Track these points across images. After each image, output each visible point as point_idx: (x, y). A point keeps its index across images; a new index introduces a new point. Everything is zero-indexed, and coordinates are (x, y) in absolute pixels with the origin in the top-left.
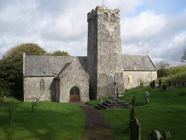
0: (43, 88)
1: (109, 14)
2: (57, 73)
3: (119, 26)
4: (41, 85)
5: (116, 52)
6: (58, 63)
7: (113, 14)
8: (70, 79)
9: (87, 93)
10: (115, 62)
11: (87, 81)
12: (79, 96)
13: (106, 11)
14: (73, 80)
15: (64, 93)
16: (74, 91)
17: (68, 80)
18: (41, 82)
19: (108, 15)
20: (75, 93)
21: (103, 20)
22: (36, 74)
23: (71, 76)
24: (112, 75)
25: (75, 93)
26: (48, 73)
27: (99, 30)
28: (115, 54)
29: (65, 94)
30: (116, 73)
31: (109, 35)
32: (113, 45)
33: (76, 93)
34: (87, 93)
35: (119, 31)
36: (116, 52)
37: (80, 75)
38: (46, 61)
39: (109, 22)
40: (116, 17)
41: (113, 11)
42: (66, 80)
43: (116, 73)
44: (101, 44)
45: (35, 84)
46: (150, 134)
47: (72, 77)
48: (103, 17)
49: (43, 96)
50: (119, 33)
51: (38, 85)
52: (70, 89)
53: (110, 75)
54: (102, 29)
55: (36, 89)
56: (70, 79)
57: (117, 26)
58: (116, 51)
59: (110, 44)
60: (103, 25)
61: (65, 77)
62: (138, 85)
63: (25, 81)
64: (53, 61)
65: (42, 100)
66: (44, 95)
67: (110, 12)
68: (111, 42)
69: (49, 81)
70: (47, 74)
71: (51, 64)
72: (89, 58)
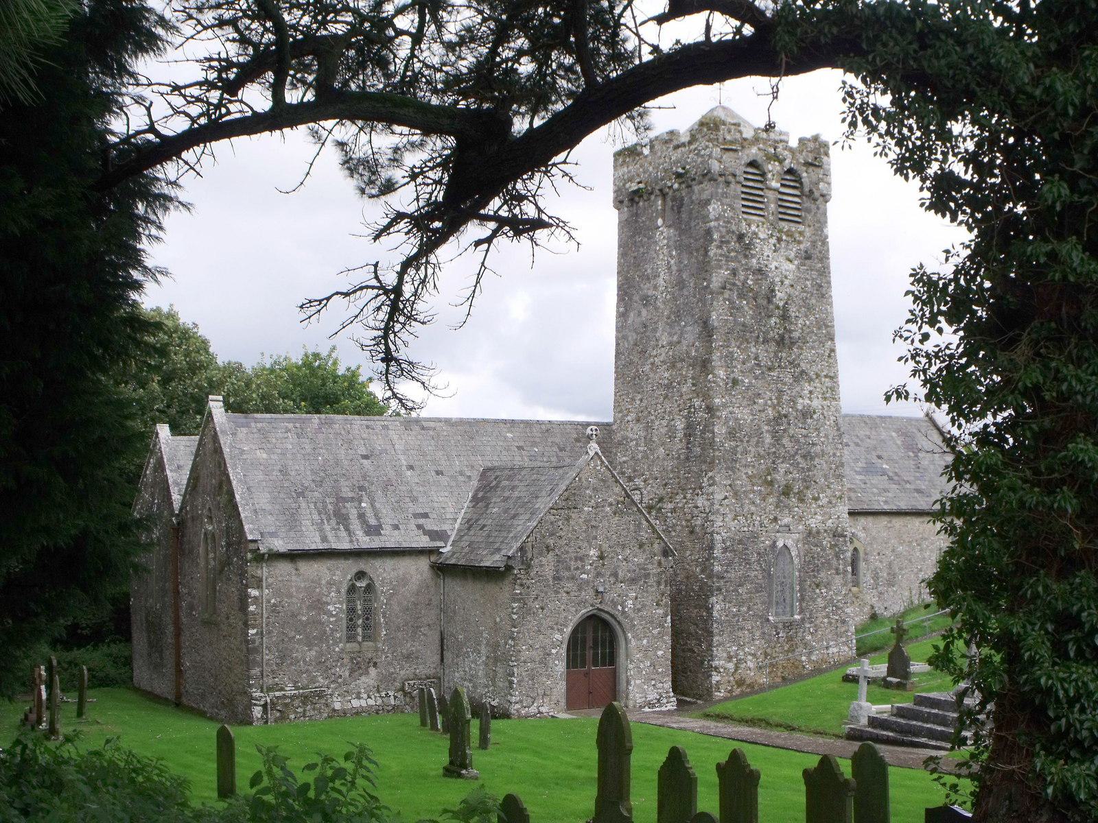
1: (773, 167)
2: (446, 527)
3: (824, 242)
4: (351, 610)
5: (807, 401)
7: (790, 171)
8: (568, 569)
9: (660, 653)
10: (803, 464)
11: (659, 583)
13: (754, 150)
14: (585, 576)
16: (590, 643)
17: (557, 578)
18: (352, 589)
19: (770, 176)
20: (589, 654)
22: (324, 539)
24: (790, 543)
25: (589, 654)
26: (396, 527)
27: (720, 267)
28: (807, 414)
29: (543, 662)
33: (595, 655)
34: (660, 653)
35: (824, 272)
36: (807, 401)
37: (624, 547)
39: (771, 218)
40: (806, 190)
41: (791, 150)
42: (549, 572)
44: (730, 356)
45: (319, 605)
47: (581, 559)
48: (740, 189)
49: (363, 678)
50: (821, 289)
51: (336, 606)
52: (568, 630)
53: (780, 544)
54: (735, 259)
55: (323, 637)
56: (568, 569)
57: (814, 243)
60: (741, 237)
65: (363, 703)
66: (373, 671)
69: (404, 581)
70: (390, 539)
71: (399, 474)
72: (635, 432)
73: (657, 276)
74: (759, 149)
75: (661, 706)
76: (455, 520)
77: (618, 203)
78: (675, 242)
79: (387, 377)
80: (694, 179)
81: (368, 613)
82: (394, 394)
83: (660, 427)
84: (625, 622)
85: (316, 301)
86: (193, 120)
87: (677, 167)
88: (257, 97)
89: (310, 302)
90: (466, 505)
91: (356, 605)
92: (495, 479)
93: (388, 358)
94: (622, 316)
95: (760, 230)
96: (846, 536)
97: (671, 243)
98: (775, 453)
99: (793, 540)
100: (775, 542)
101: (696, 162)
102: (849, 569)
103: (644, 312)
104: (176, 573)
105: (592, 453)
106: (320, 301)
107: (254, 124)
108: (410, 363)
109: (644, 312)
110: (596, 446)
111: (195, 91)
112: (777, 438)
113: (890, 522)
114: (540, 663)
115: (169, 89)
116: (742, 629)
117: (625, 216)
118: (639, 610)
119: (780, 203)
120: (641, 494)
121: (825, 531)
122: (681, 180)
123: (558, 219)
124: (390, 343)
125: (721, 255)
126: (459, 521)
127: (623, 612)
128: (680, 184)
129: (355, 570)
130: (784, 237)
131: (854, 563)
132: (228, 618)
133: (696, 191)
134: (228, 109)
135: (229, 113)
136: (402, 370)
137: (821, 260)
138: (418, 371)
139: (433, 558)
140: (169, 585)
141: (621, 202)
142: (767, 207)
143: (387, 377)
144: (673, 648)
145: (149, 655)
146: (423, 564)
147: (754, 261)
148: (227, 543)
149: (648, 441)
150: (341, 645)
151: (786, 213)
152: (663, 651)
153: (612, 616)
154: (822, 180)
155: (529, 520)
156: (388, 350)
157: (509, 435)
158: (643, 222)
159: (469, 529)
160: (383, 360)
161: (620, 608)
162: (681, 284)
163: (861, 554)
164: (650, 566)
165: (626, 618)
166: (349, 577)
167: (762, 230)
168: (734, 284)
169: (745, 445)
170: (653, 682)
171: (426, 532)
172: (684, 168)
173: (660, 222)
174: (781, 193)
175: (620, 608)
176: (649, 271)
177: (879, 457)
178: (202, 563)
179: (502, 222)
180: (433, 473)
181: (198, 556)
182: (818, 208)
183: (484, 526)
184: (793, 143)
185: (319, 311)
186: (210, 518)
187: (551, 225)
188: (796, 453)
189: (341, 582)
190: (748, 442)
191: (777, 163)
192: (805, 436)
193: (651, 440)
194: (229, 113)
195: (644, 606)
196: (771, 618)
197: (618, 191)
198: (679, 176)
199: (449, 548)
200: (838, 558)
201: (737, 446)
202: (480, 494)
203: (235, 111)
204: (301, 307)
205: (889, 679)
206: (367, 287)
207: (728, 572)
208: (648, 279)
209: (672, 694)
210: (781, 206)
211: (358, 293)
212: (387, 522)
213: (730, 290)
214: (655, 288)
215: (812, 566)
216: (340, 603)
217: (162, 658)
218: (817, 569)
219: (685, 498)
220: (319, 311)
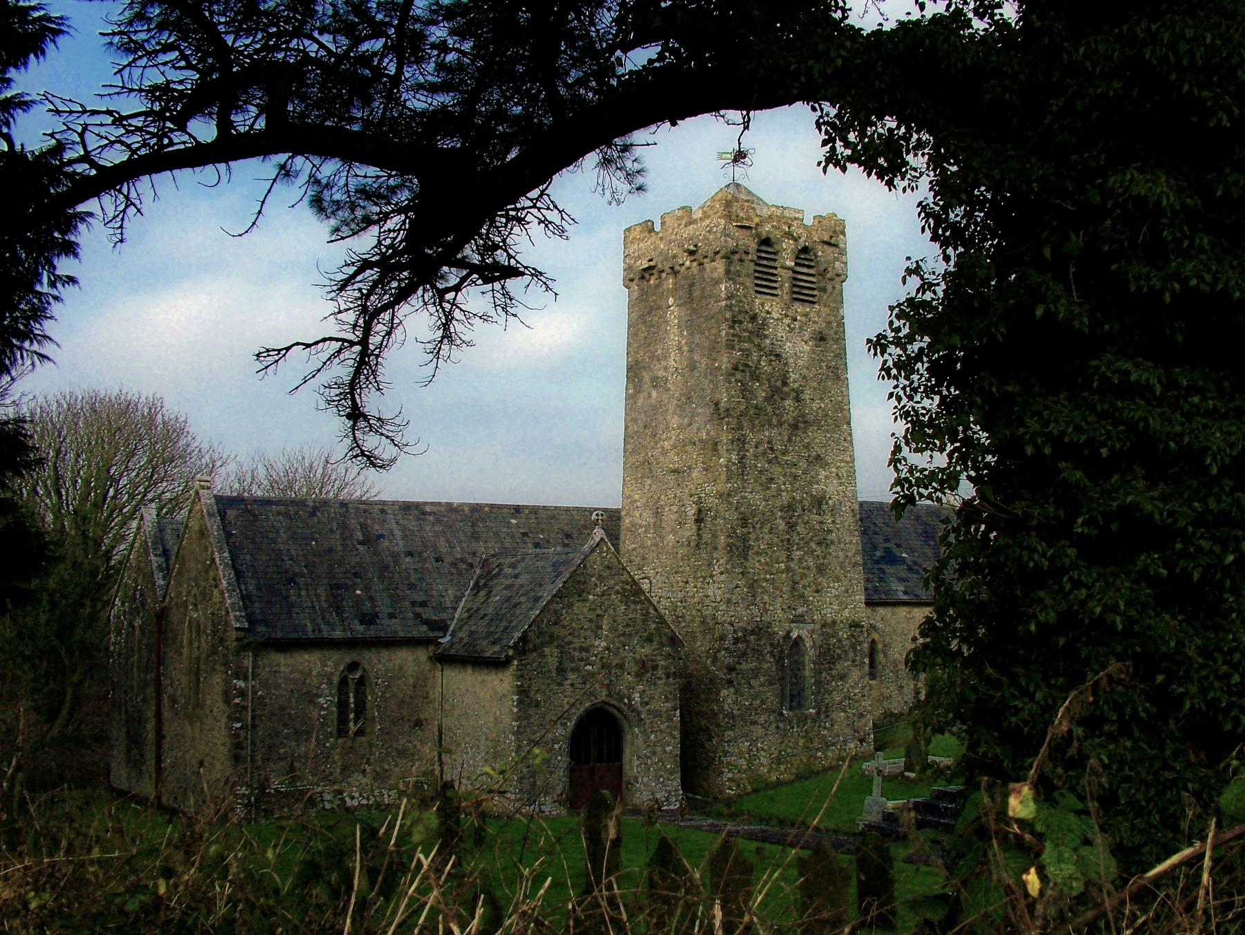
3: (841, 324)
4: (342, 706)
6: (435, 548)
9: (668, 749)
11: (668, 676)
14: (589, 668)
17: (561, 670)
18: (344, 682)
21: (749, 283)
23: (577, 643)
24: (804, 633)
31: (785, 384)
32: (807, 447)
34: (668, 749)
42: (552, 662)
46: (1228, 782)
58: (828, 485)
59: (790, 440)
61: (547, 650)
62: (918, 693)
64: (405, 537)
67: (789, 235)
68: (795, 427)
70: (396, 627)
73: (666, 358)
75: (669, 805)
76: (455, 609)
77: (628, 282)
78: (687, 321)
79: (354, 434)
80: (706, 257)
81: (360, 709)
82: (362, 452)
83: (670, 516)
84: (631, 715)
85: (274, 350)
86: (134, 152)
87: (690, 245)
88: (204, 130)
89: (268, 351)
90: (467, 593)
91: (349, 698)
92: (497, 567)
93: (356, 414)
94: (631, 399)
95: (772, 308)
96: (863, 626)
97: (682, 323)
98: (789, 540)
99: (808, 631)
100: (788, 633)
101: (708, 239)
102: (867, 660)
103: (654, 394)
104: (160, 661)
105: (598, 539)
106: (279, 351)
107: (198, 156)
108: (379, 419)
109: (654, 394)
110: (602, 532)
111: (138, 122)
112: (791, 526)
113: (910, 613)
115: (109, 120)
116: (754, 723)
117: (635, 295)
118: (647, 703)
119: (794, 282)
120: (651, 583)
121: (842, 622)
122: (692, 258)
123: (533, 269)
124: (357, 396)
125: (734, 335)
126: (459, 610)
127: (630, 705)
128: (692, 261)
129: (348, 660)
130: (798, 318)
131: (872, 654)
132: (212, 711)
133: (708, 269)
134: (170, 139)
135: (171, 143)
136: (371, 426)
137: (837, 341)
138: (387, 428)
139: (431, 648)
140: (151, 676)
141: (632, 280)
142: (781, 286)
143: (354, 434)
144: (682, 743)
145: (129, 751)
146: (422, 655)
147: (768, 341)
148: (213, 631)
149: (658, 526)
151: (801, 294)
152: (672, 747)
153: (618, 709)
154: (836, 259)
155: (532, 609)
156: (355, 406)
157: (514, 521)
158: (653, 301)
159: (469, 617)
160: (349, 416)
161: (626, 701)
162: (692, 367)
163: (880, 646)
164: (659, 658)
165: (633, 711)
166: (342, 668)
167: (776, 309)
168: (747, 365)
169: (758, 531)
170: (661, 780)
171: (426, 622)
172: (696, 246)
173: (671, 301)
174: (795, 272)
175: (626, 701)
176: (659, 352)
177: (898, 546)
178: (185, 651)
179: (473, 269)
180: (433, 560)
181: (182, 646)
182: (834, 288)
183: (485, 615)
184: (809, 221)
185: (277, 361)
186: (195, 605)
187: (523, 274)
188: (811, 540)
189: (332, 674)
190: (761, 528)
191: (791, 242)
192: (821, 523)
193: (660, 526)
194: (171, 143)
195: (652, 698)
196: (784, 712)
197: (628, 269)
198: (691, 253)
199: (448, 638)
200: (854, 649)
201: (749, 533)
202: (482, 582)
203: (180, 141)
204: (258, 355)
205: (907, 774)
206: (331, 339)
207: (740, 664)
208: (659, 360)
209: (681, 792)
210: (795, 286)
211: (321, 344)
212: (384, 607)
213: (743, 371)
214: (666, 369)
215: (827, 657)
216: (331, 695)
217: (142, 755)
218: (833, 661)
219: (695, 587)
220: (277, 361)
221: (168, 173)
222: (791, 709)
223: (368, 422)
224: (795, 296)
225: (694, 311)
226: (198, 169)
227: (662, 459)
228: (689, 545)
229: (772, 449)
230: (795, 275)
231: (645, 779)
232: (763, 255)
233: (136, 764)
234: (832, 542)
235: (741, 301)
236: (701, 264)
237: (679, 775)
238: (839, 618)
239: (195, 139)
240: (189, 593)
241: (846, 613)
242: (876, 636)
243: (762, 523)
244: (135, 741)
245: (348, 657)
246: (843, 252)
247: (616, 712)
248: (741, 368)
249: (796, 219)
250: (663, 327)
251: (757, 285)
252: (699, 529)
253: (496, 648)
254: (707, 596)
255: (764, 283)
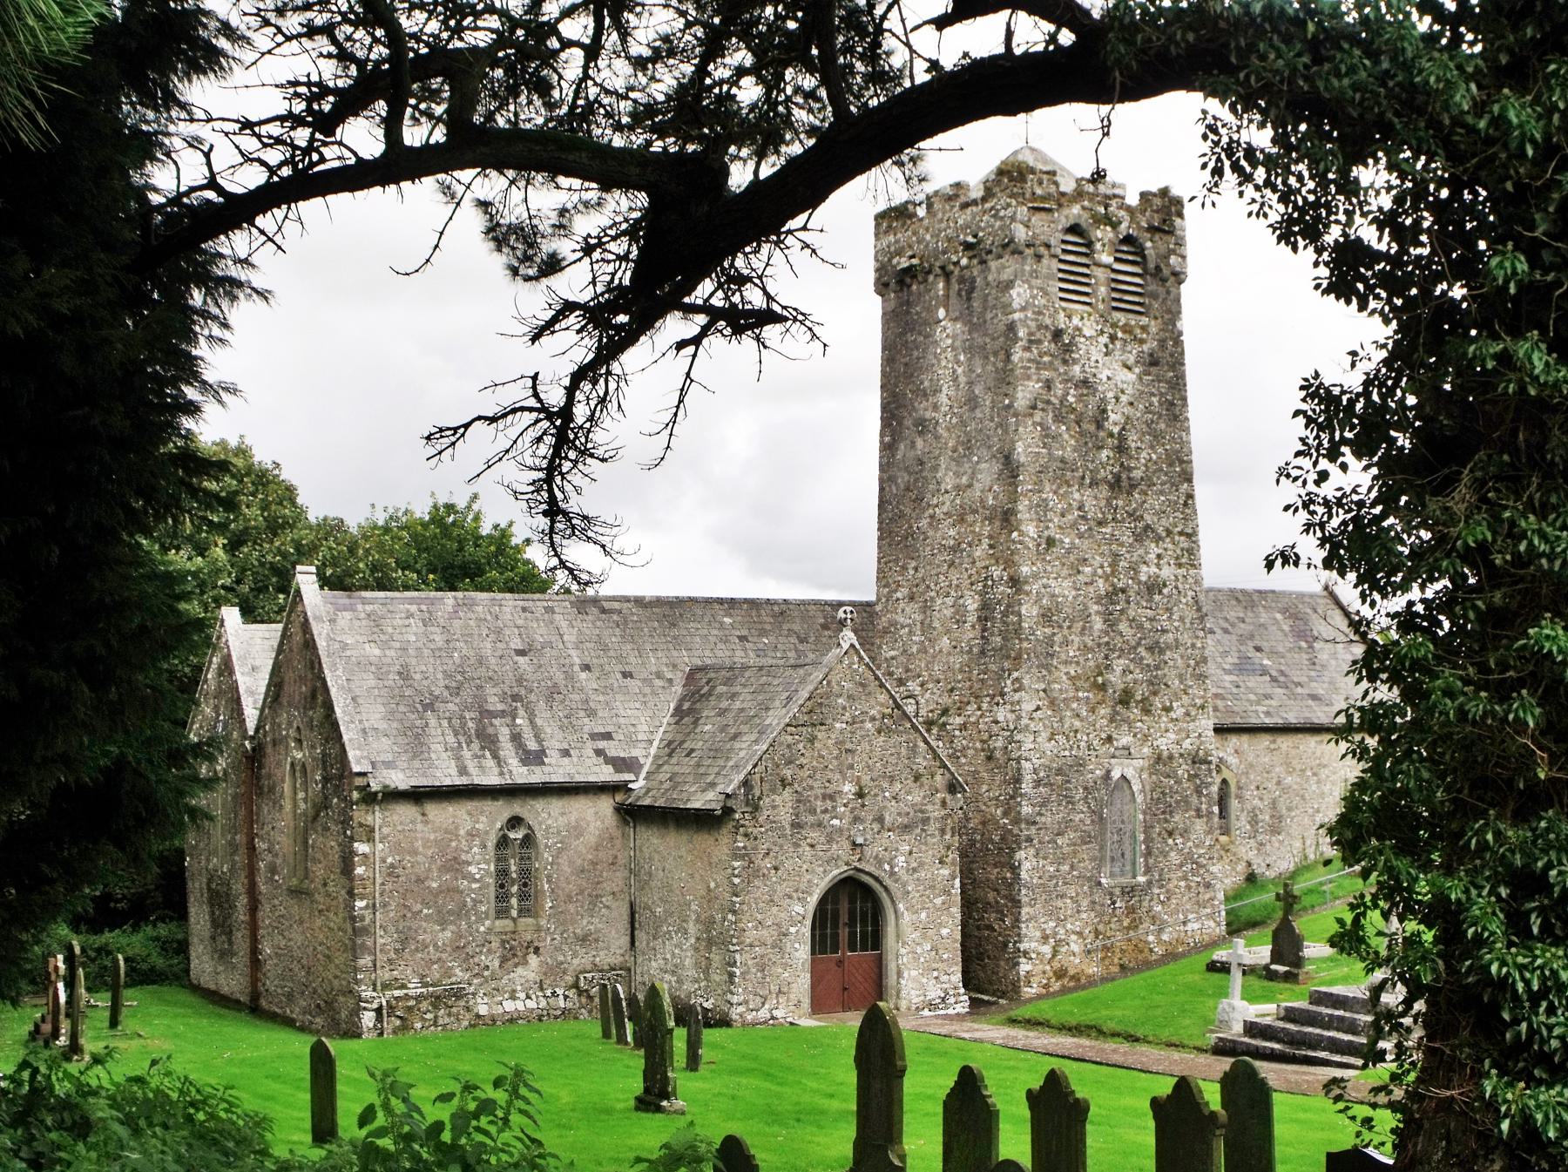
0: (523, 897)
1: (1103, 234)
3: (1178, 342)
4: (502, 873)
5: (1154, 569)
7: (1128, 240)
8: (813, 812)
9: (945, 932)
11: (943, 832)
12: (879, 965)
14: (836, 822)
15: (767, 935)
17: (796, 825)
18: (503, 842)
19: (1098, 246)
20: (844, 933)
25: (844, 933)
30: (1159, 759)
33: (852, 935)
34: (945, 932)
36: (1154, 569)
38: (517, 644)
39: (1101, 306)
40: (1151, 265)
42: (785, 816)
43: (1159, 759)
44: (1043, 505)
45: (455, 865)
47: (832, 798)
48: (1055, 265)
49: (520, 970)
51: (481, 867)
52: (813, 900)
53: (1116, 774)
54: (1051, 365)
55: (461, 911)
56: (813, 812)
63: (370, 840)
65: (520, 1006)
66: (533, 960)
69: (577, 830)
70: (557, 770)
73: (937, 391)
74: (1084, 208)
76: (651, 742)
77: (882, 287)
79: (551, 538)
81: (526, 878)
86: (272, 171)
89: (441, 430)
90: (665, 721)
93: (553, 510)
98: (1107, 644)
102: (1216, 809)
103: (920, 443)
105: (846, 646)
106: (455, 429)
107: (359, 176)
108: (585, 518)
110: (851, 635)
111: (275, 129)
112: (1111, 622)
114: (773, 947)
117: (892, 304)
118: (914, 870)
122: (971, 253)
125: (1029, 360)
126: (656, 744)
127: (892, 873)
128: (970, 258)
129: (506, 815)
130: (1120, 335)
131: (1223, 801)
132: (325, 885)
134: (321, 154)
135: (323, 160)
136: (573, 527)
139: (619, 798)
143: (551, 538)
144: (964, 925)
146: (605, 806)
147: (1077, 368)
150: (487, 923)
152: (951, 928)
153: (876, 879)
154: (1173, 252)
155: (756, 742)
156: (552, 500)
161: (887, 867)
164: (929, 808)
166: (498, 825)
168: (1048, 402)
172: (975, 236)
173: (941, 313)
174: (1114, 271)
176: (926, 384)
177: (1258, 649)
178: (288, 806)
179: (714, 314)
181: (282, 796)
185: (453, 444)
186: (299, 741)
188: (1139, 644)
189: (487, 833)
192: (1151, 620)
193: (930, 626)
194: (323, 160)
195: (921, 864)
196: (1103, 881)
202: (686, 706)
203: (332, 157)
204: (428, 438)
205: (1273, 967)
206: (523, 409)
208: (925, 395)
209: (962, 991)
211: (510, 417)
214: (936, 407)
216: (487, 862)
217: (230, 943)
218: (1169, 811)
220: (453, 444)
221: (320, 199)
222: (1112, 875)
223: (570, 520)
224: (1114, 304)
225: (973, 327)
226: (358, 194)
227: (931, 533)
228: (970, 652)
229: (1083, 518)
230: (1113, 276)
231: (914, 973)
232: (1070, 248)
233: (224, 955)
234: (1168, 647)
235: (1040, 313)
236: (983, 262)
237: (959, 968)
238: (1175, 750)
239: (355, 154)
240: (290, 724)
241: (1187, 744)
242: (1226, 774)
243: (1072, 621)
244: (222, 925)
245: (501, 811)
246: (1180, 243)
247: (884, 895)
248: (1040, 406)
249: (1115, 196)
250: (931, 349)
251: (1061, 290)
252: (984, 630)
253: (711, 795)
254: (997, 722)
255: (1071, 287)
